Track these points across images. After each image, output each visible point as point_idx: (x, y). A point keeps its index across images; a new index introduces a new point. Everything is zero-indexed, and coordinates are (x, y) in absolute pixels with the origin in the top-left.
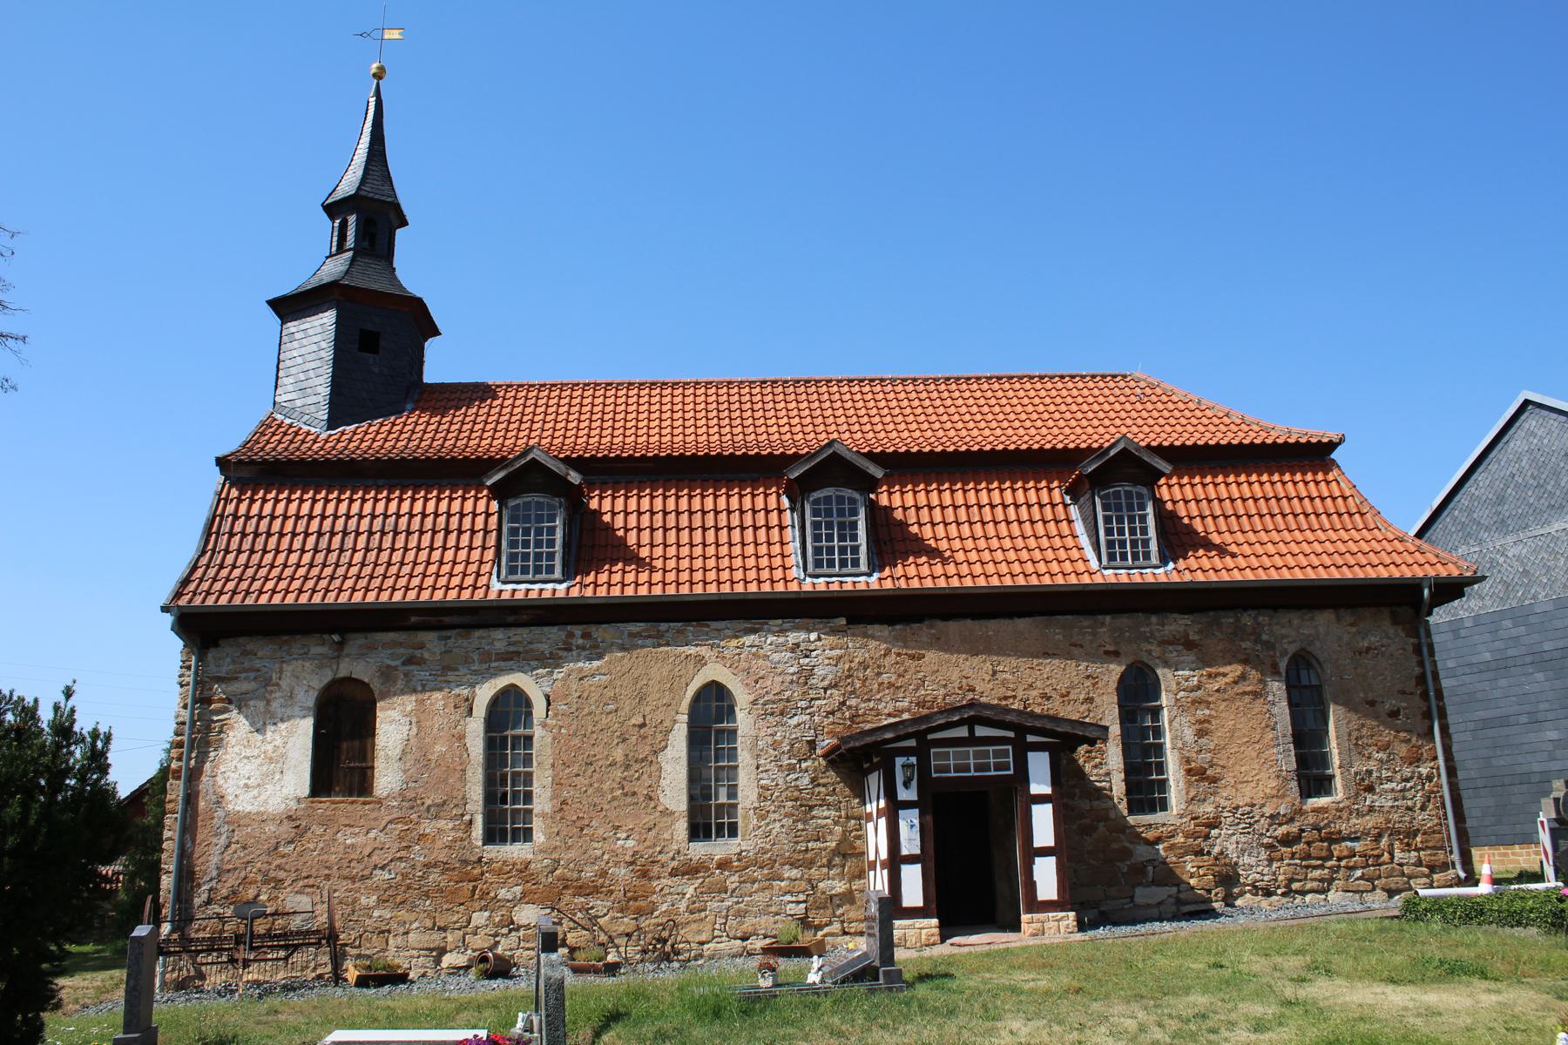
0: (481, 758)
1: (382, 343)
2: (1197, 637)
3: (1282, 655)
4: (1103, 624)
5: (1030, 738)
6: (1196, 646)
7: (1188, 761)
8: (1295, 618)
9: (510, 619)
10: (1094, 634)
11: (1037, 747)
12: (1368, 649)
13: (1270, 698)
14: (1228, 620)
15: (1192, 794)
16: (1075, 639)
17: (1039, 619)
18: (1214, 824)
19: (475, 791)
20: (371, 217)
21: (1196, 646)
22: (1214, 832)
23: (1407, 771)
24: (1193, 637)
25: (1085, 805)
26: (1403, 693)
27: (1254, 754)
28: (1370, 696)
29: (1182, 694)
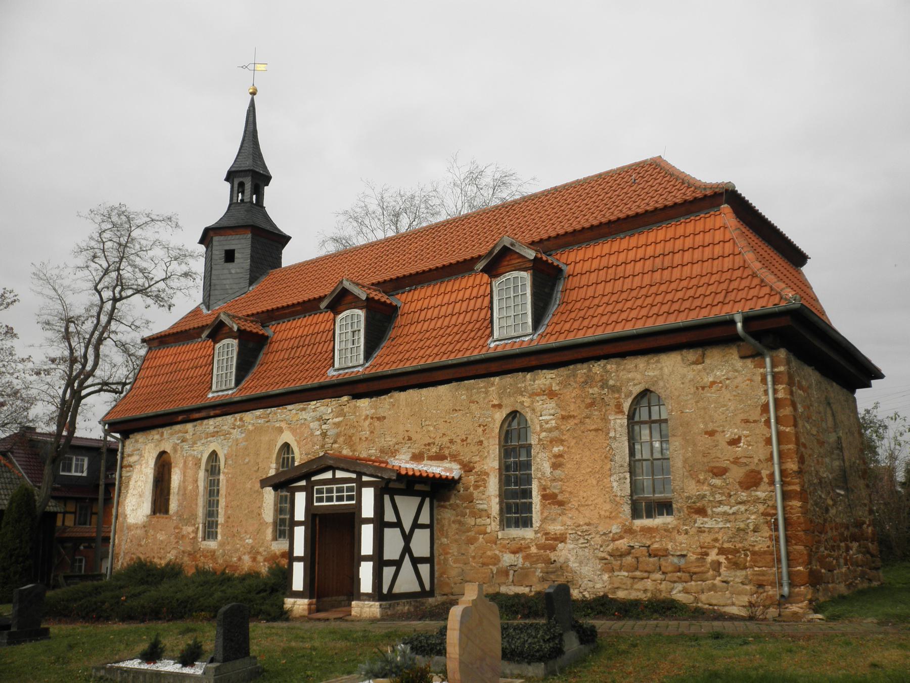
0: (171, 497)
1: (236, 255)
2: (557, 388)
3: (627, 396)
4: (493, 384)
5: (365, 479)
6: (556, 395)
7: (544, 489)
8: (641, 362)
9: (197, 415)
10: (486, 393)
11: (368, 484)
12: (713, 383)
13: (612, 434)
14: (582, 370)
15: (545, 514)
16: (474, 398)
17: (454, 384)
18: (562, 539)
19: (200, 512)
20: (249, 175)
21: (556, 395)
22: (561, 546)
23: (744, 495)
24: (555, 388)
25: (471, 521)
26: (747, 421)
27: (595, 482)
28: (711, 427)
29: (544, 434)
